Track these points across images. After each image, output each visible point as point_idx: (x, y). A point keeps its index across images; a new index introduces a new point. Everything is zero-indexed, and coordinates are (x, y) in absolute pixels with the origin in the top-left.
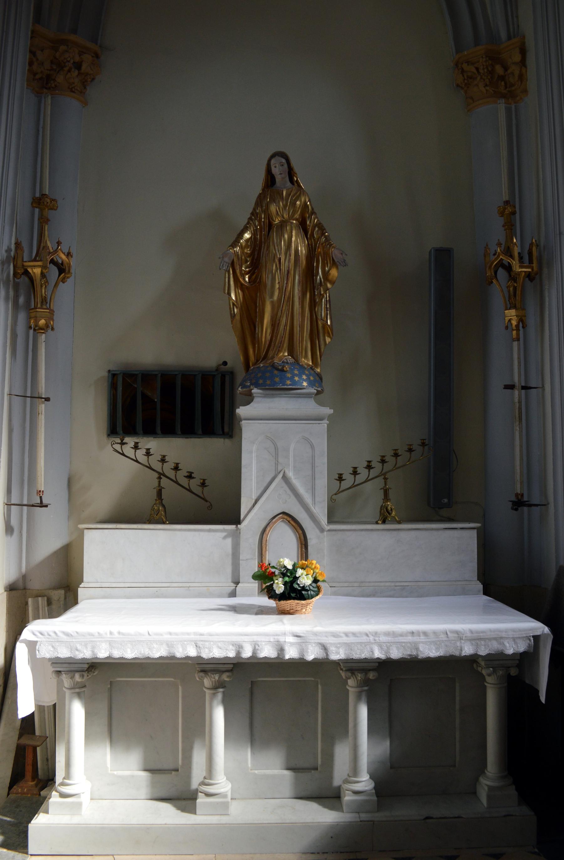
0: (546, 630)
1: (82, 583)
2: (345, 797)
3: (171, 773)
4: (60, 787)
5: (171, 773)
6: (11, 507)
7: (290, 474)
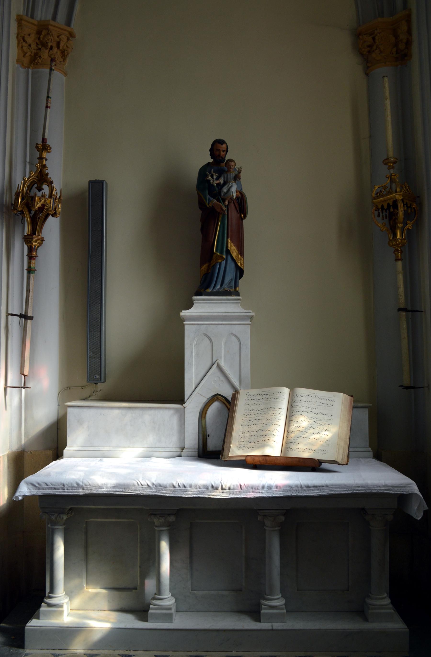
0: (415, 488)
1: (66, 447)
2: (262, 610)
3: (132, 591)
4: (46, 599)
5: (132, 591)
6: (22, 390)
7: (222, 364)
